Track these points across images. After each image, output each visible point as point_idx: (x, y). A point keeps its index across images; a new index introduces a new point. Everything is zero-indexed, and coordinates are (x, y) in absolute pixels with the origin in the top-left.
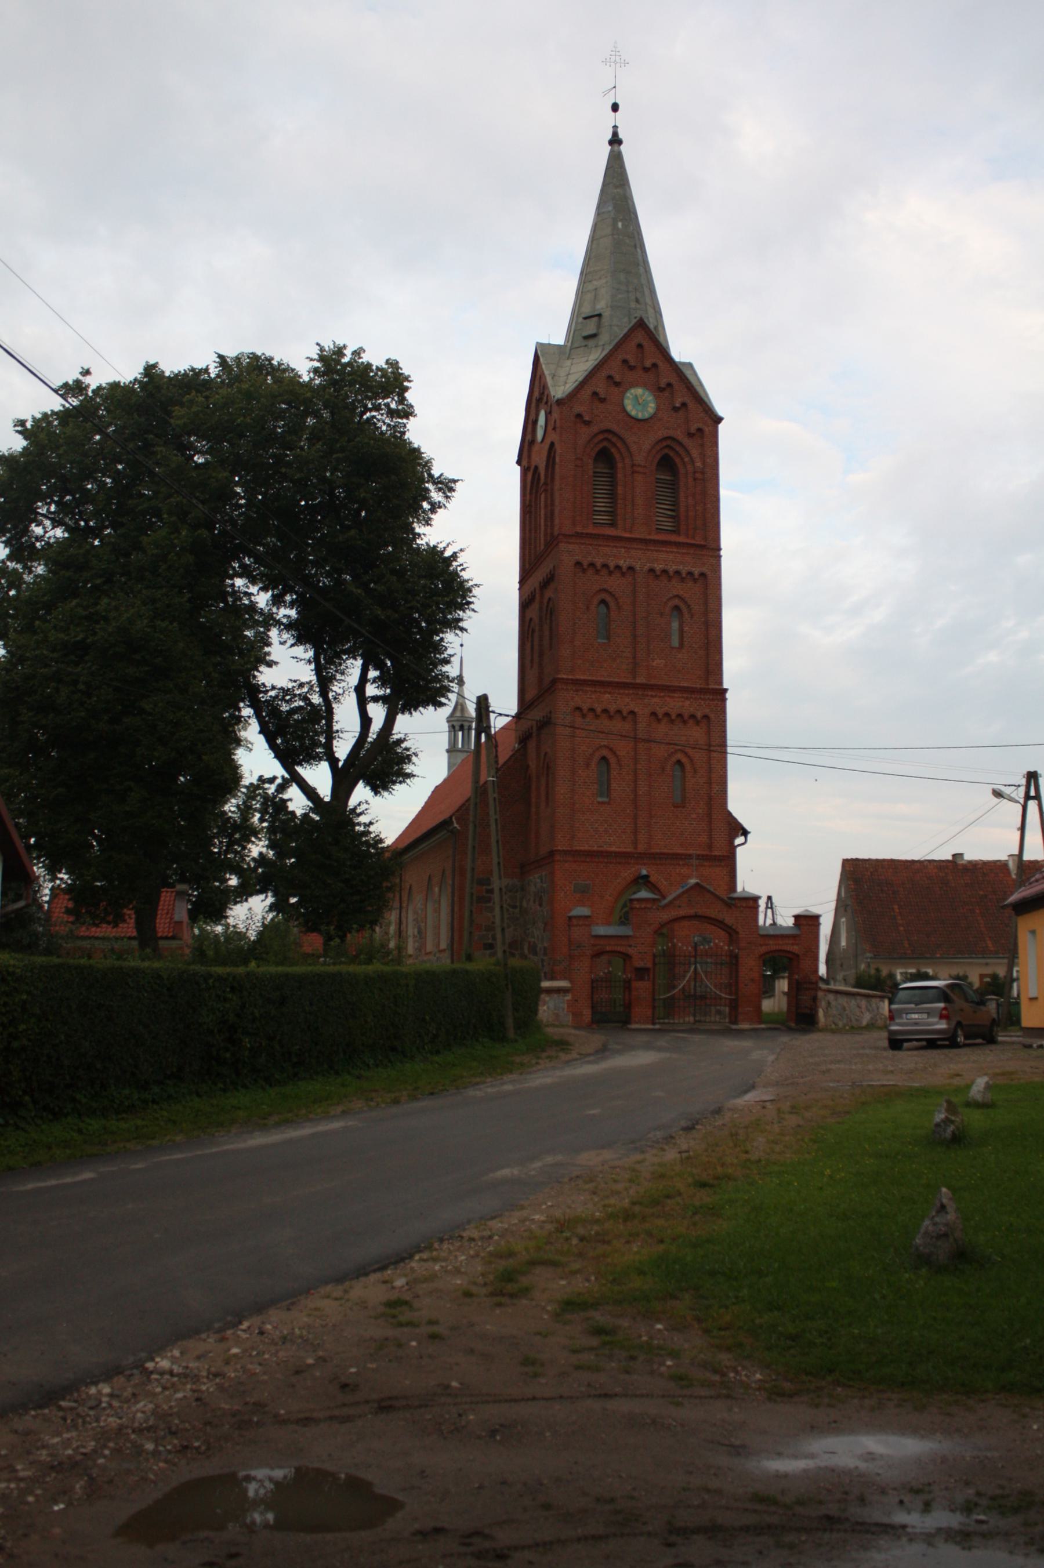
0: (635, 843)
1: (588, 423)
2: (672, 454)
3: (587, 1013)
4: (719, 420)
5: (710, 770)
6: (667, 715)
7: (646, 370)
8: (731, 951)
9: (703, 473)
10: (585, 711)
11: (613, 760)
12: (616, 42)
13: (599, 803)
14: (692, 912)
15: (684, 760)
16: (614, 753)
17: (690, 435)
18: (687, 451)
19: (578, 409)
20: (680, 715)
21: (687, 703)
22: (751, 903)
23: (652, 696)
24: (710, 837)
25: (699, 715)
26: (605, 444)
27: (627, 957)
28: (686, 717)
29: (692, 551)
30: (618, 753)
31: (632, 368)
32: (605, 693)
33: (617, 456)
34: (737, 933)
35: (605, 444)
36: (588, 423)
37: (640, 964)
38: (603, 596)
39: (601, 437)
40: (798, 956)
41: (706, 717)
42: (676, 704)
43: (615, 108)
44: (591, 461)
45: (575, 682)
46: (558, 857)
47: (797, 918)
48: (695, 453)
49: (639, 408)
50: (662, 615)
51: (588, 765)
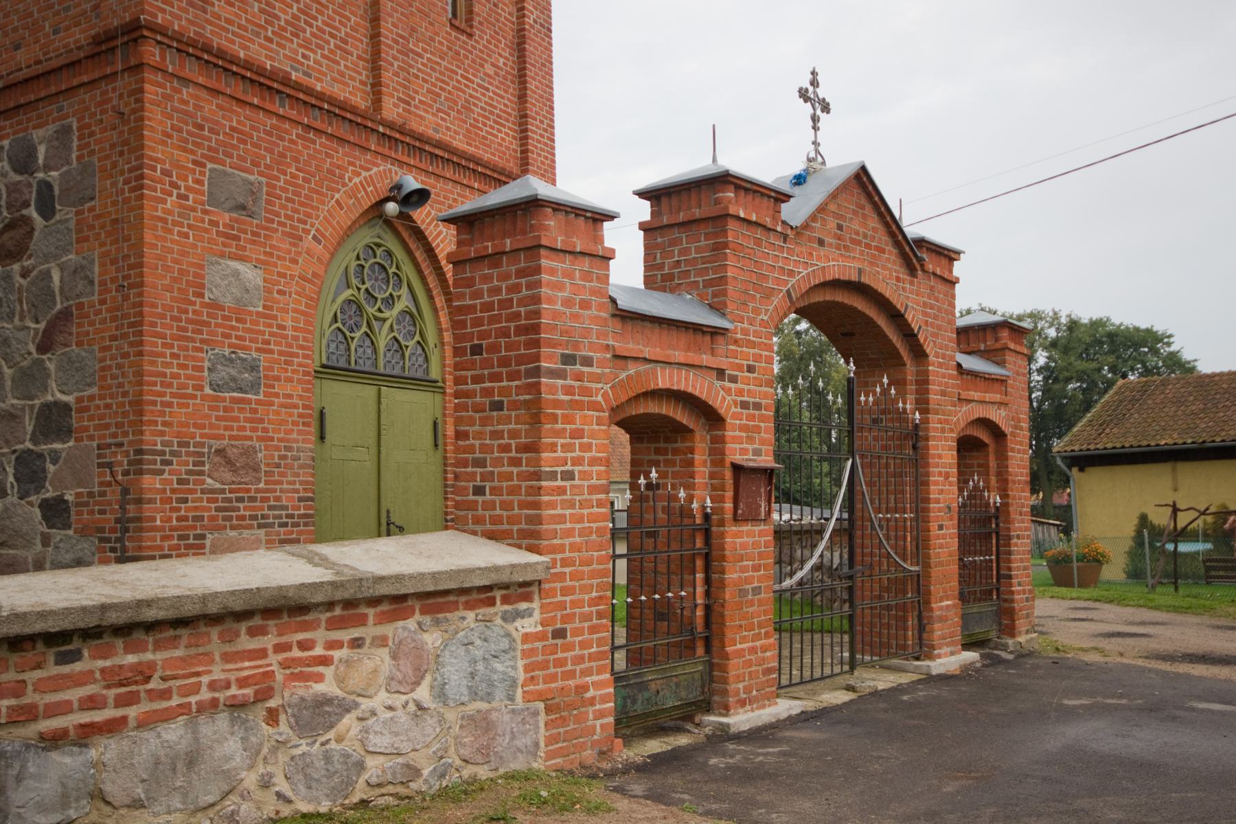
34: (919, 354)
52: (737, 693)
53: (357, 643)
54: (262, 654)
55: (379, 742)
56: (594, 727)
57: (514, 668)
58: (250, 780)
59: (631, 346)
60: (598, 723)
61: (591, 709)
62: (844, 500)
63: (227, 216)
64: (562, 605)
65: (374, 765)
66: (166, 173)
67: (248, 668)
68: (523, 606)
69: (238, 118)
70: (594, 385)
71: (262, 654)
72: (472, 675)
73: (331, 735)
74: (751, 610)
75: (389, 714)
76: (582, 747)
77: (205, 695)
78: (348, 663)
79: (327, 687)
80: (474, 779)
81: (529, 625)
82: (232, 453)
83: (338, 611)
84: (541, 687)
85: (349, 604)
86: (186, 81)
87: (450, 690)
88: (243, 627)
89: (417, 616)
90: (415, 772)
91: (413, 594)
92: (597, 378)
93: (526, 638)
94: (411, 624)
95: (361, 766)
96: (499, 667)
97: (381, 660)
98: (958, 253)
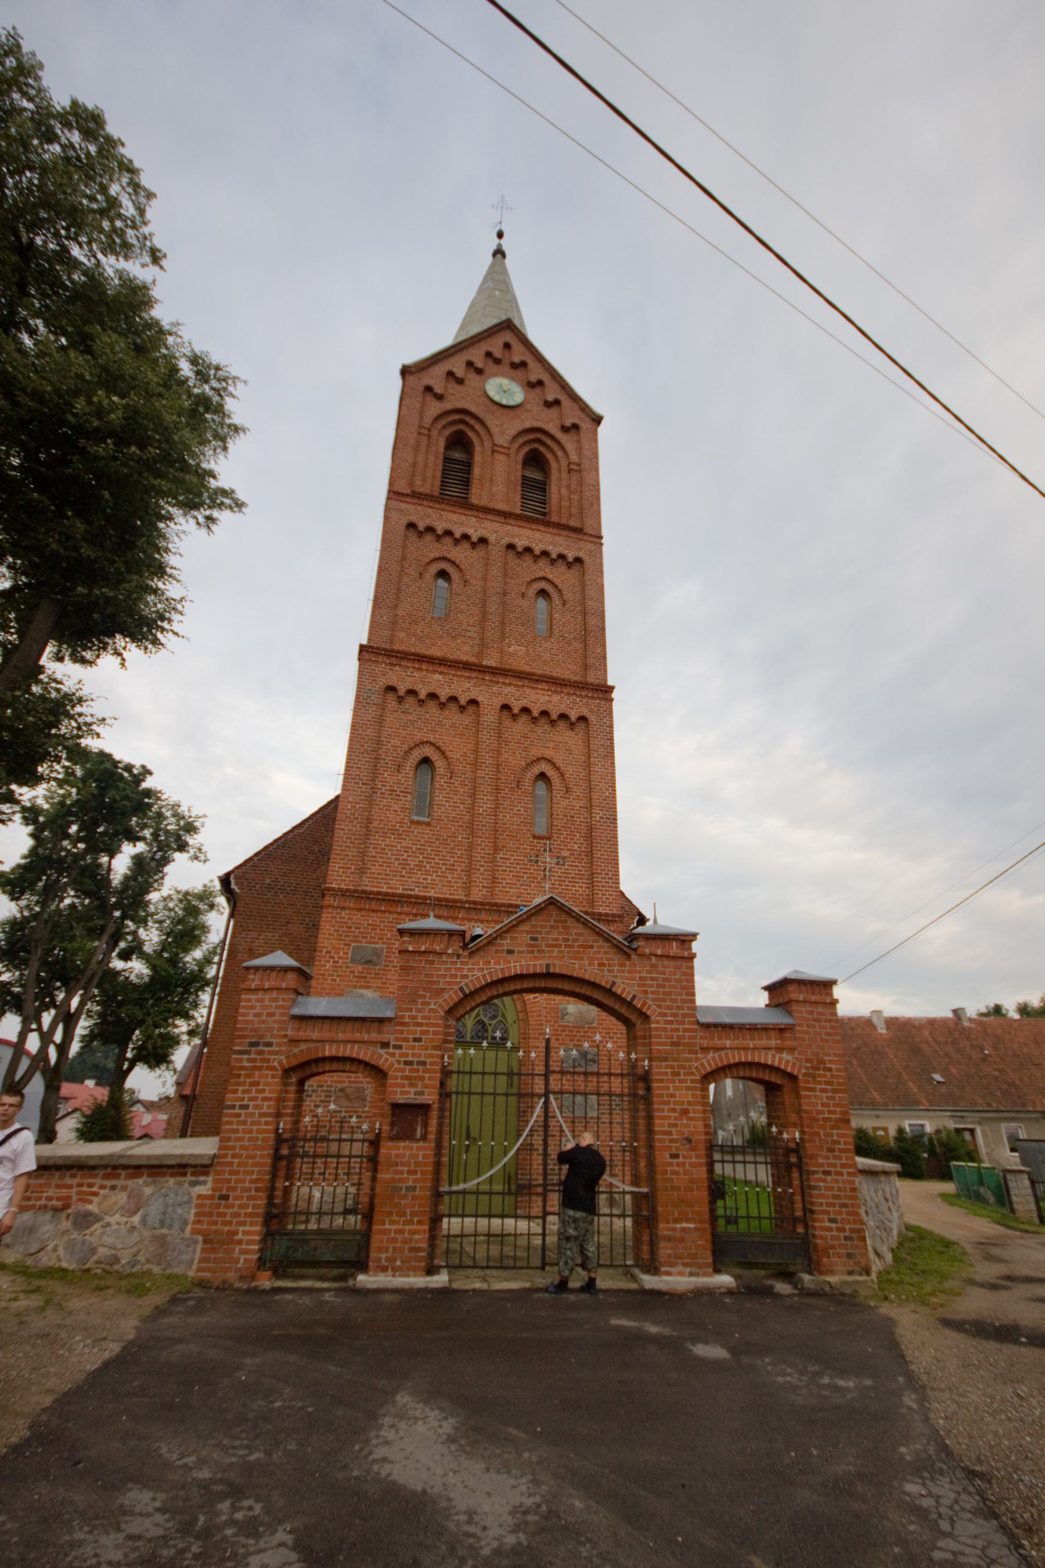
1: (440, 397)
2: (542, 449)
4: (598, 420)
5: (583, 602)
6: (525, 710)
7: (514, 366)
8: (633, 1065)
9: (579, 465)
11: (439, 763)
13: (412, 822)
14: (538, 965)
15: (550, 772)
16: (443, 753)
17: (565, 429)
18: (563, 449)
20: (544, 713)
21: (556, 698)
22: (674, 949)
23: (504, 684)
24: (591, 885)
26: (462, 427)
30: (449, 754)
31: (498, 362)
32: (434, 672)
34: (646, 1018)
36: (440, 397)
38: (443, 565)
40: (793, 1078)
41: (582, 719)
42: (538, 699)
43: (500, 235)
47: (770, 988)
50: (523, 595)
51: (399, 768)
52: (379, 1260)
54: (70, 1187)
55: (108, 1240)
56: (239, 1259)
57: (188, 1213)
60: (242, 1258)
61: (237, 1248)
63: (360, 968)
64: (229, 1181)
65: (102, 1252)
66: (327, 952)
67: (63, 1192)
68: (202, 1178)
70: (272, 1057)
71: (70, 1187)
72: (164, 1213)
73: (87, 1232)
74: (403, 1202)
75: (116, 1227)
76: (228, 1270)
77: (43, 1202)
78: (105, 1197)
80: (149, 1272)
81: (203, 1190)
82: (349, 1091)
83: (109, 1170)
84: (205, 1227)
85: (115, 1167)
86: (344, 908)
88: (69, 1173)
89: (145, 1178)
91: (145, 1166)
92: (276, 1053)
93: (199, 1197)
94: (141, 1181)
95: (94, 1251)
96: (179, 1211)
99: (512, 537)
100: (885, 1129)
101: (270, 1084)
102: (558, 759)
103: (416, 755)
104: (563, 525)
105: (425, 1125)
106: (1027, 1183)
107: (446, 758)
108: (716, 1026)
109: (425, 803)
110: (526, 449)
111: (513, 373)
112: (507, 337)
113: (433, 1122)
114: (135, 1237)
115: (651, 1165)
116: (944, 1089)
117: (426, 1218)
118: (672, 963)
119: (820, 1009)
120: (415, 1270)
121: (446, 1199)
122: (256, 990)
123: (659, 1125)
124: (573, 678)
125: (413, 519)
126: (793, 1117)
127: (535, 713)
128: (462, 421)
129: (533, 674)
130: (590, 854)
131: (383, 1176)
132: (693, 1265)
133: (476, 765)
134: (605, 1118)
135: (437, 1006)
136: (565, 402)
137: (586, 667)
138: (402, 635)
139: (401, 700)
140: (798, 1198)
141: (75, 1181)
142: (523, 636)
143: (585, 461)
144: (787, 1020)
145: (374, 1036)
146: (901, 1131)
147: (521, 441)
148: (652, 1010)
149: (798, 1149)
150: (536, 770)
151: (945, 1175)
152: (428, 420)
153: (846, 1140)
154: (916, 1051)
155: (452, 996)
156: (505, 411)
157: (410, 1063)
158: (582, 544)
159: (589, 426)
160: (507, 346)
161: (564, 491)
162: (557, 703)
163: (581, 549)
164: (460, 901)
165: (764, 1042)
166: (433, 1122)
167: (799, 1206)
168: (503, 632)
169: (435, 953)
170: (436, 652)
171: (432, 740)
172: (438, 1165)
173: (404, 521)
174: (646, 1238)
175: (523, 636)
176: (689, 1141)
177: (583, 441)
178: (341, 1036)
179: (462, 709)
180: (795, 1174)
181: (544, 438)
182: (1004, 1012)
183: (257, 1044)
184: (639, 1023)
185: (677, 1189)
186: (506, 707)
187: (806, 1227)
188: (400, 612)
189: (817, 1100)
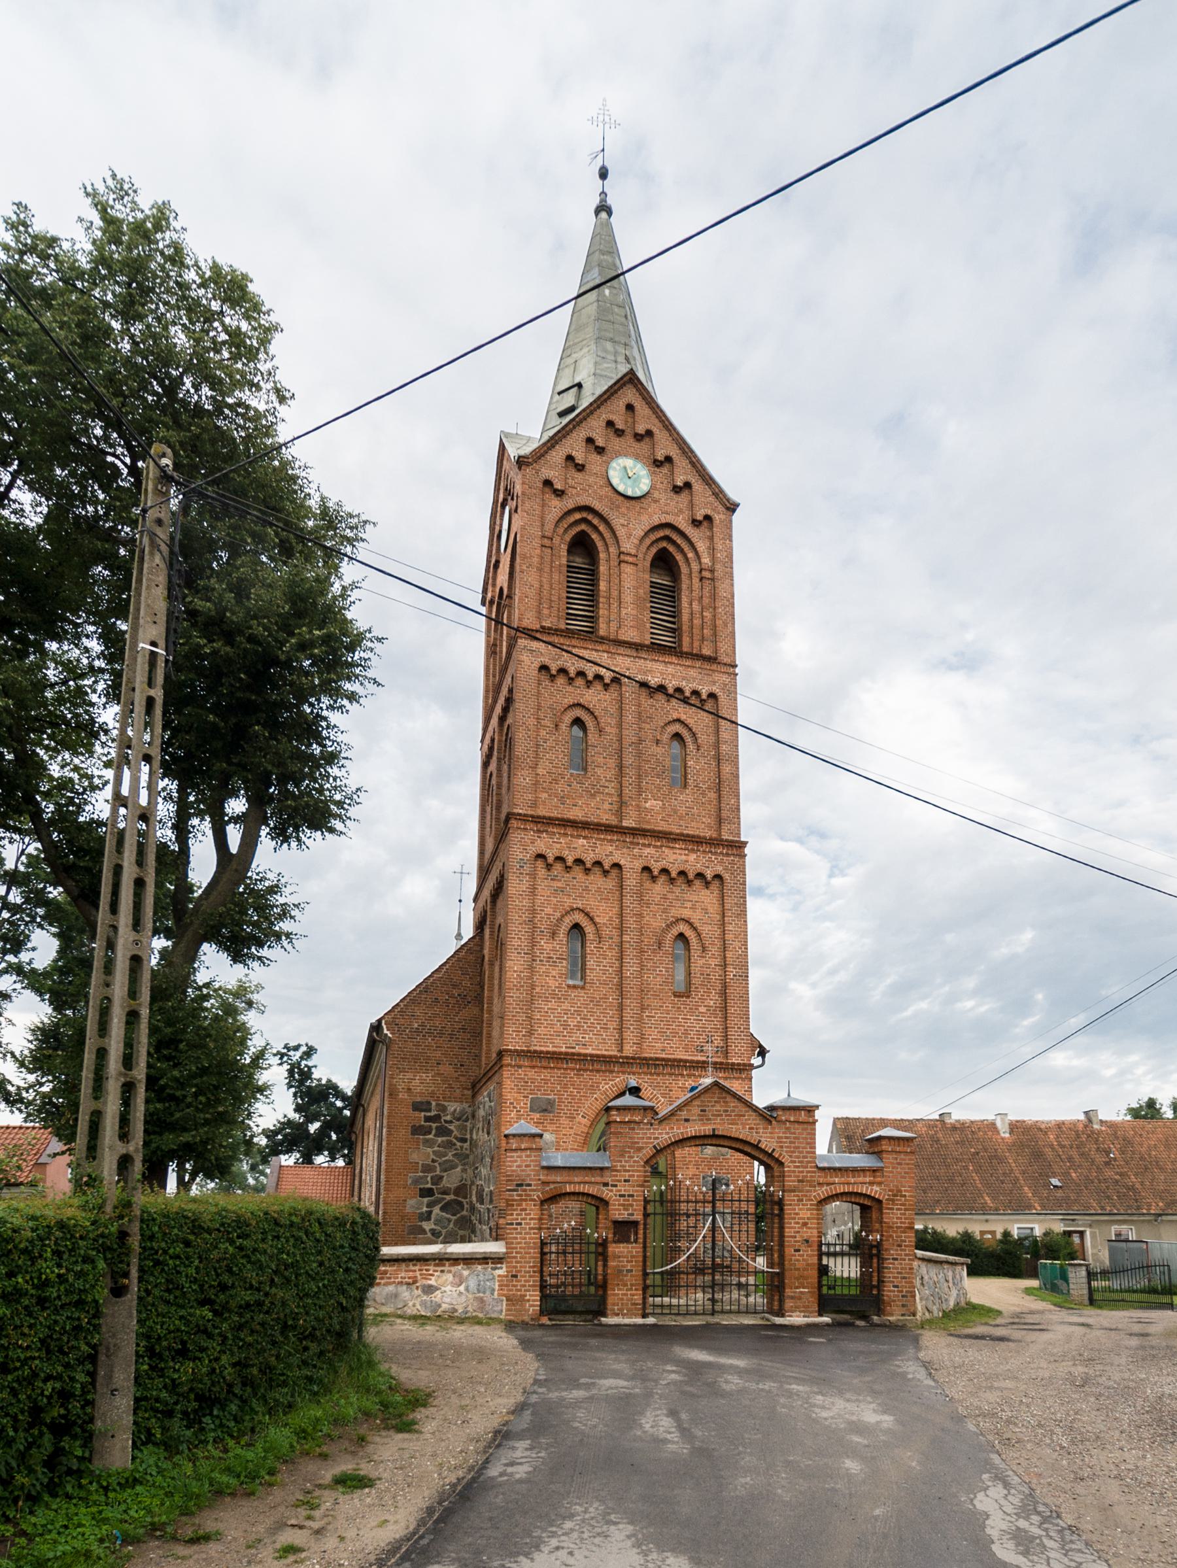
0: (621, 1046)
2: (671, 549)
3: (533, 1298)
4: (732, 508)
7: (638, 437)
9: (712, 571)
10: (550, 860)
11: (589, 929)
12: (604, 100)
13: (569, 986)
14: (707, 1129)
15: (689, 933)
16: (592, 919)
17: (696, 523)
19: (547, 473)
20: (682, 873)
21: (693, 857)
23: (644, 845)
25: (709, 874)
26: (583, 527)
27: (601, 1203)
28: (691, 876)
29: (698, 664)
30: (597, 920)
31: (620, 433)
32: (579, 837)
33: (599, 544)
34: (781, 1164)
35: (583, 527)
36: (559, 494)
37: (620, 1214)
39: (578, 516)
40: (879, 1202)
42: (676, 858)
43: (603, 174)
44: (564, 547)
45: (537, 820)
46: (507, 1060)
48: (701, 546)
49: (629, 482)
50: (658, 742)
51: (554, 934)
53: (442, 1271)
55: (447, 1300)
58: (411, 1304)
59: (552, 1178)
62: (414, 1243)
63: (538, 1115)
69: (545, 1074)
79: (432, 1282)
81: (502, 1272)
85: (441, 1260)
86: (520, 1067)
87: (471, 1288)
90: (456, 1311)
95: (440, 1306)
97: (450, 1277)
98: (817, 1107)
99: (645, 673)
100: (993, 1233)
101: (533, 1211)
102: (695, 918)
103: (568, 922)
104: (697, 655)
105: (636, 1234)
106: (1084, 1273)
107: (595, 924)
108: (829, 1169)
109: (579, 967)
110: (654, 550)
111: (637, 445)
112: (629, 395)
113: (641, 1232)
114: (463, 1299)
115: (782, 1256)
116: (1059, 1194)
117: (640, 1287)
118: (801, 1127)
119: (902, 1156)
120: (636, 1315)
121: (651, 1276)
122: (516, 1150)
123: (788, 1232)
124: (708, 835)
125: (546, 660)
126: (877, 1226)
127: (674, 874)
128: (584, 520)
129: (671, 833)
130: (725, 1009)
131: (611, 1263)
132: (806, 1312)
133: (621, 929)
134: (736, 1228)
135: (639, 1158)
136: (698, 486)
137: (720, 821)
138: (545, 795)
139: (549, 867)
140: (875, 1274)
141: (417, 1268)
142: (659, 788)
143: (718, 566)
144: (880, 1165)
145: (598, 1179)
146: (1006, 1234)
147: (648, 541)
148: (786, 1159)
149: (879, 1245)
150: (675, 931)
151: (1033, 1274)
152: (549, 526)
153: (911, 1238)
154: (1038, 1155)
155: (648, 1152)
156: (627, 504)
157: (623, 1196)
158: (716, 676)
159: (723, 517)
160: (630, 407)
161: (696, 607)
162: (693, 861)
163: (714, 683)
164: (615, 1057)
165: (861, 1179)
166: (641, 1232)
167: (875, 1279)
168: (640, 787)
169: (635, 1122)
170: (576, 814)
171: (580, 906)
172: (645, 1257)
173: (536, 665)
174: (776, 1298)
175: (659, 788)
176: (807, 1241)
177: (716, 540)
178: (576, 1179)
179: (606, 873)
180: (875, 1260)
181: (674, 536)
182: (1158, 1106)
183: (521, 1185)
184: (776, 1167)
185: (798, 1269)
186: (646, 869)
187: (879, 1291)
188: (540, 771)
189: (893, 1216)
